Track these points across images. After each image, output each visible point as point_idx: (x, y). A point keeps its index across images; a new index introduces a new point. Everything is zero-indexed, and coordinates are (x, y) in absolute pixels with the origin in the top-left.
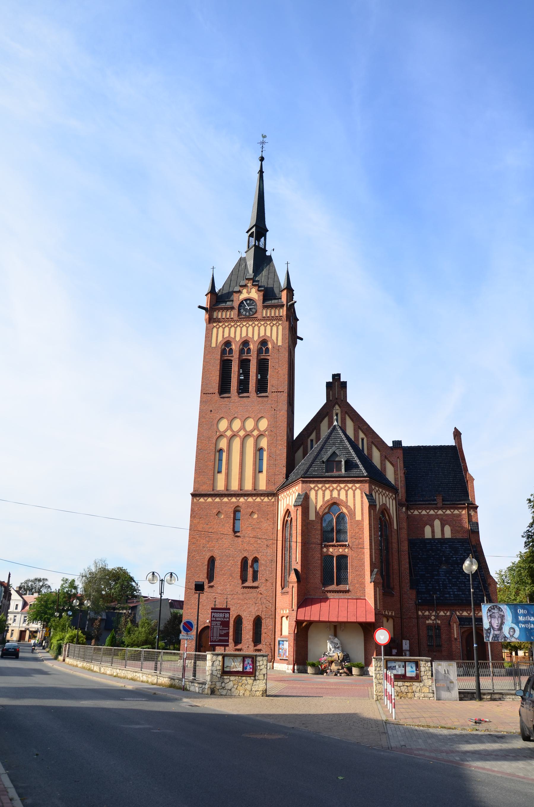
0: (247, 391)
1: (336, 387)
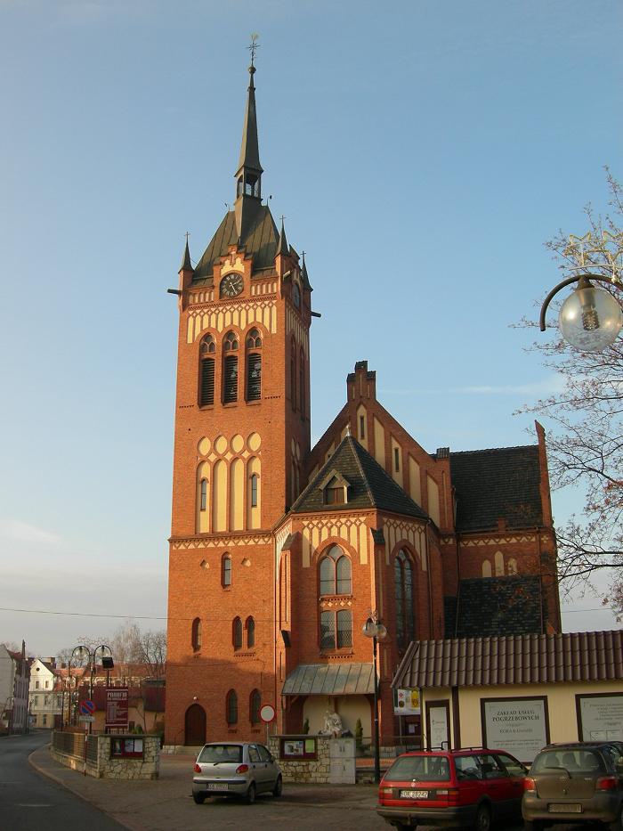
0: (235, 400)
1: (362, 380)
